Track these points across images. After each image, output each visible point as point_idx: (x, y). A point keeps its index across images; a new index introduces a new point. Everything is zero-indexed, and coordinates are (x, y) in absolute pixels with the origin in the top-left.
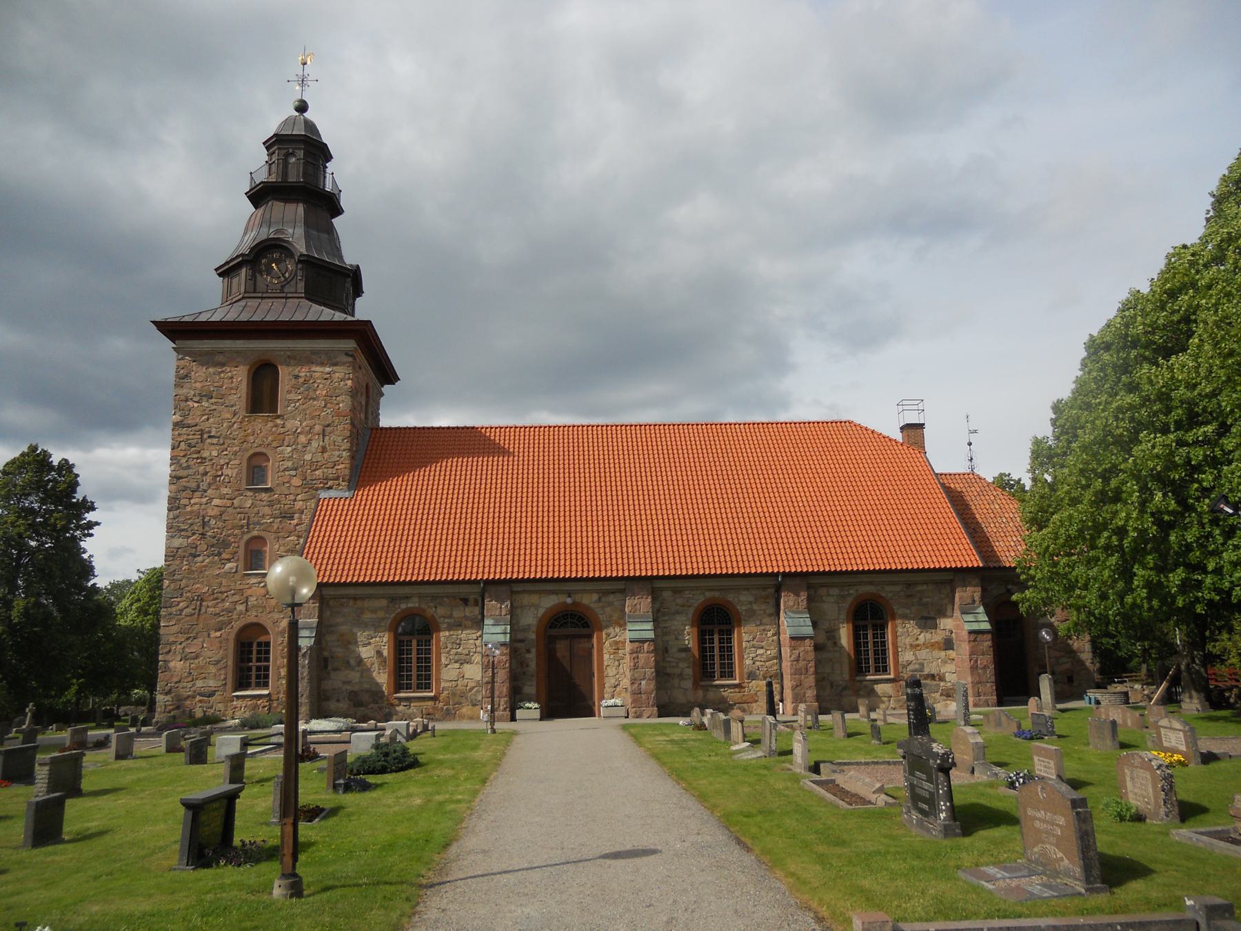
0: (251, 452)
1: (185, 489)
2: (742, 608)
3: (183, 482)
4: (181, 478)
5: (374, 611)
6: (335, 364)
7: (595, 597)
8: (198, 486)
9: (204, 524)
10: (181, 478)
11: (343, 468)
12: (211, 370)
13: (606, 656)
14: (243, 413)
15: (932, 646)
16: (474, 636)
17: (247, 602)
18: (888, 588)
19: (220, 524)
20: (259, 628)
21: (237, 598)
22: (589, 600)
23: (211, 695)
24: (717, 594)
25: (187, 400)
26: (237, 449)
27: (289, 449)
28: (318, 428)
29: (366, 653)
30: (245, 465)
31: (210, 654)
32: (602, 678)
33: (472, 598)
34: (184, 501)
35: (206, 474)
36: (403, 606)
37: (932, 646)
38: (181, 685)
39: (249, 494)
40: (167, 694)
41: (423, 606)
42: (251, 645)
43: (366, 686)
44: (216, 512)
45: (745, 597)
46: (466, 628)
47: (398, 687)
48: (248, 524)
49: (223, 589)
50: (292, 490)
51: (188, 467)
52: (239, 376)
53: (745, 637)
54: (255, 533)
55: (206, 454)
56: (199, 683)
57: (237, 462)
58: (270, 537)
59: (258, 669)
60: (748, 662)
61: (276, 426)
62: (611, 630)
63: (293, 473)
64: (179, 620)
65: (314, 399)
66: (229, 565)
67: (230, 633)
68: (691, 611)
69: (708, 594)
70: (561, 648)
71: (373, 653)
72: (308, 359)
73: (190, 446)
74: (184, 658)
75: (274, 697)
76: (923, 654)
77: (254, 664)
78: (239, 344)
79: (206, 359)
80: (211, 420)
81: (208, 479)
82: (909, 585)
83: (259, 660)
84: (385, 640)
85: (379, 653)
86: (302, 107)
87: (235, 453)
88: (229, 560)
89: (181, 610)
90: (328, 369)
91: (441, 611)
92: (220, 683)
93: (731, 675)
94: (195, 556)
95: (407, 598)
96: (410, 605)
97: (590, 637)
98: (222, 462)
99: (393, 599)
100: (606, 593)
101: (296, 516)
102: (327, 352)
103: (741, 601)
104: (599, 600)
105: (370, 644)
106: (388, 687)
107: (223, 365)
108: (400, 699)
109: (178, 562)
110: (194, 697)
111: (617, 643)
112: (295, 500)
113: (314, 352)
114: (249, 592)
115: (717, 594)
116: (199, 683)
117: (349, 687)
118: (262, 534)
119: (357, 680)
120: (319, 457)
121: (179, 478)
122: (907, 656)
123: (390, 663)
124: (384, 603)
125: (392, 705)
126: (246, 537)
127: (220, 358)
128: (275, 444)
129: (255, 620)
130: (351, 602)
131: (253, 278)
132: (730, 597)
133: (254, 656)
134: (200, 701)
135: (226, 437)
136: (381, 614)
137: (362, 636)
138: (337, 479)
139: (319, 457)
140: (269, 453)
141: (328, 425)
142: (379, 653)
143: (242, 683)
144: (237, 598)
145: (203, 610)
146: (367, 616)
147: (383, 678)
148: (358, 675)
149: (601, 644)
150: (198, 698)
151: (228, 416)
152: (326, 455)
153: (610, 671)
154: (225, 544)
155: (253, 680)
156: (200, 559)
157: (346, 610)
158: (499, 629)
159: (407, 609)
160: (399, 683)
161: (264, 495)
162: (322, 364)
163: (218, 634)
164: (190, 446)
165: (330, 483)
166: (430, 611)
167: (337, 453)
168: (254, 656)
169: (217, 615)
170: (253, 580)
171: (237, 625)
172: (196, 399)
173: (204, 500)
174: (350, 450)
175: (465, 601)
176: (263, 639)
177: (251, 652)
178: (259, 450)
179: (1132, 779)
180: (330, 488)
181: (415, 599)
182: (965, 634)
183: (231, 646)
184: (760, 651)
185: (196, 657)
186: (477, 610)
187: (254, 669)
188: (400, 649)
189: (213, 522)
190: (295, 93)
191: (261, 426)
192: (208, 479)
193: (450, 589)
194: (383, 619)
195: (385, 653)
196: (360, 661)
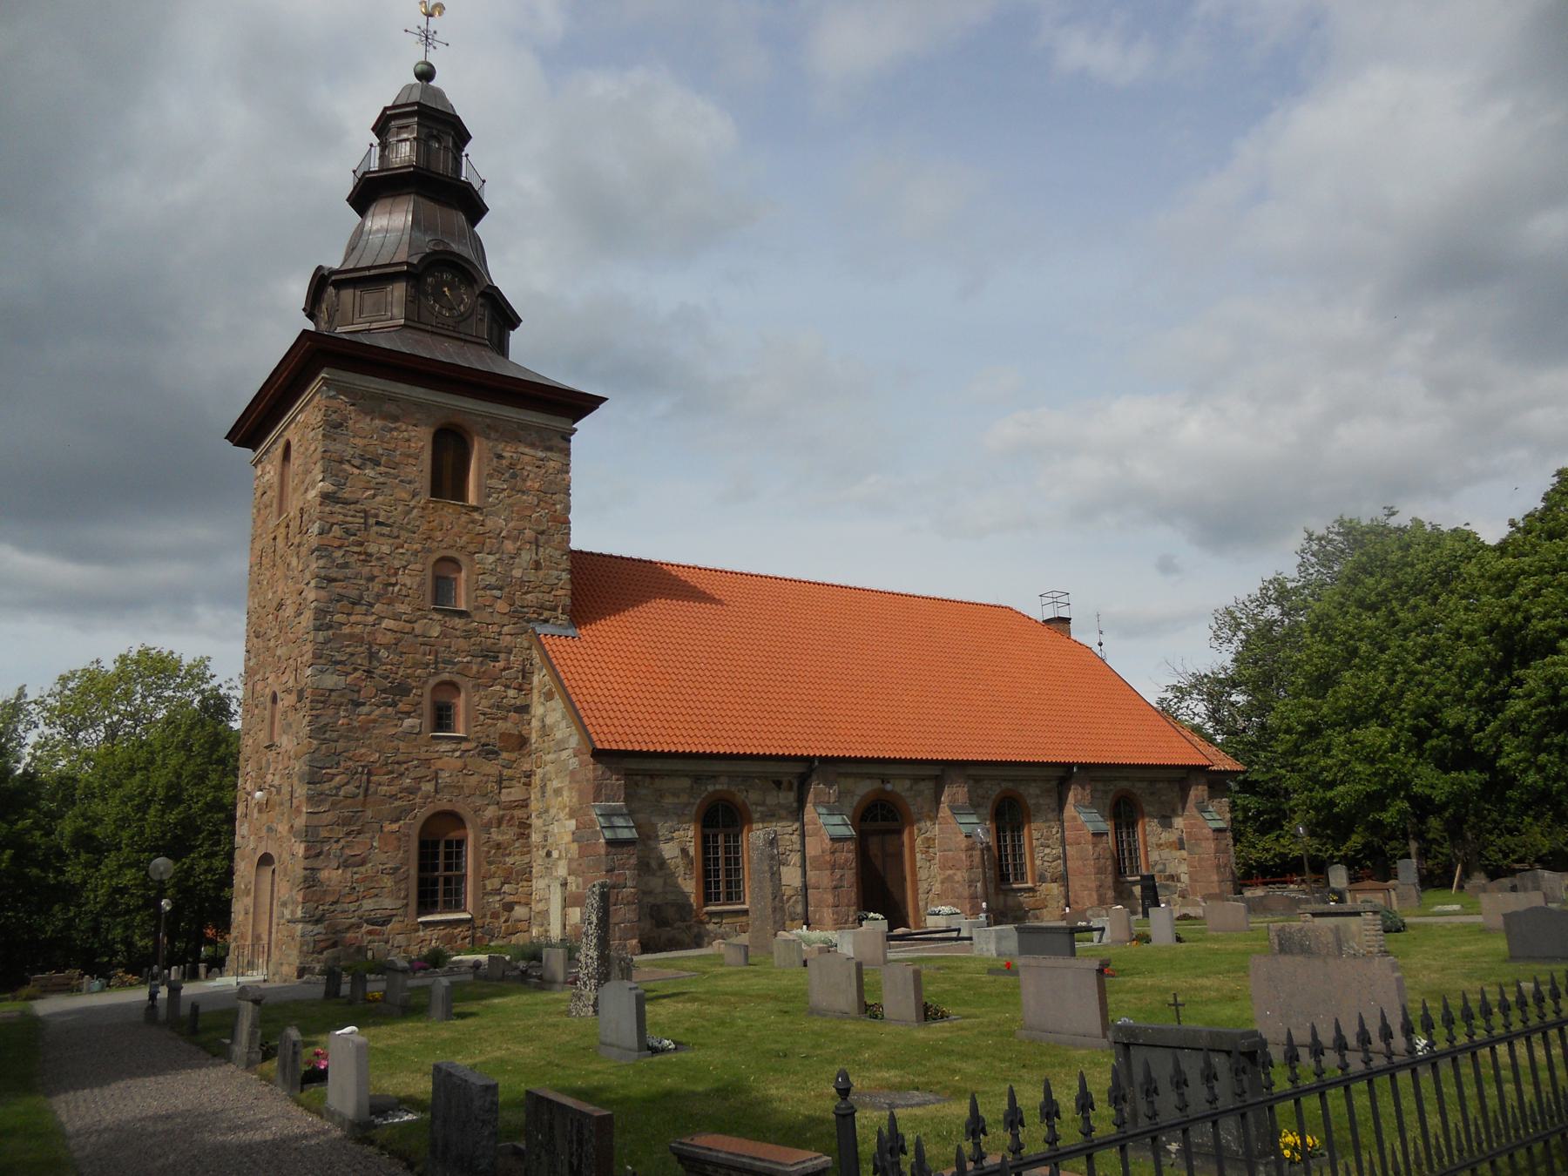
0: (437, 555)
1: (341, 597)
2: (1031, 802)
3: (337, 588)
4: (335, 580)
5: (675, 794)
6: (550, 449)
7: (907, 783)
8: (361, 597)
9: (372, 656)
10: (335, 580)
11: (563, 594)
12: (377, 422)
13: (919, 856)
14: (425, 496)
15: (1170, 845)
16: (790, 830)
17: (436, 777)
18: (1138, 785)
19: (394, 658)
20: (453, 819)
21: (421, 772)
22: (899, 787)
23: (385, 922)
24: (1010, 785)
25: (341, 462)
26: (417, 546)
27: (491, 558)
28: (529, 534)
29: (669, 851)
30: (429, 572)
31: (383, 857)
32: (915, 882)
33: (785, 780)
34: (338, 617)
35: (372, 579)
36: (710, 788)
37: (1170, 845)
38: (339, 907)
39: (437, 616)
40: (317, 922)
41: (733, 789)
42: (436, 844)
43: (671, 897)
44: (389, 638)
45: (1033, 790)
46: (781, 819)
47: (708, 897)
48: (436, 662)
49: (401, 758)
50: (497, 618)
51: (346, 565)
52: (419, 439)
53: (1036, 835)
54: (445, 676)
55: (372, 548)
56: (368, 904)
57: (418, 566)
58: (466, 684)
59: (448, 881)
60: (1038, 862)
61: (473, 522)
62: (922, 824)
63: (497, 593)
64: (334, 804)
65: (523, 492)
66: (408, 722)
67: (412, 826)
68: (990, 804)
69: (1004, 785)
70: (874, 844)
71: (677, 852)
72: (515, 434)
73: (347, 531)
74: (345, 865)
75: (479, 923)
76: (1166, 853)
77: (441, 872)
78: (419, 393)
79: (369, 404)
80: (379, 498)
81: (376, 587)
82: (1152, 781)
83: (448, 867)
84: (691, 833)
85: (684, 851)
86: (426, 74)
87: (415, 553)
88: (408, 714)
89: (338, 788)
90: (541, 454)
91: (754, 796)
92: (400, 903)
93: (1023, 880)
94: (358, 704)
95: (714, 777)
96: (718, 787)
97: (900, 832)
98: (397, 564)
99: (698, 778)
100: (917, 779)
101: (502, 656)
102: (540, 430)
103: (1032, 793)
104: (911, 789)
105: (672, 839)
106: (697, 897)
107: (395, 419)
108: (711, 914)
109: (331, 712)
110: (359, 926)
111: (928, 839)
112: (500, 634)
113: (524, 427)
114: (439, 764)
115: (1010, 785)
116: (368, 904)
117: (651, 900)
118: (456, 678)
119: (659, 890)
120: (532, 575)
121: (331, 580)
122: (1154, 856)
123: (698, 864)
124: (686, 783)
125: (702, 922)
126: (433, 682)
127: (391, 408)
128: (471, 548)
129: (448, 807)
130: (648, 781)
131: (412, 302)
132: (1022, 789)
133: (441, 861)
134: (370, 933)
135: (401, 528)
136: (684, 798)
137: (663, 829)
138: (554, 609)
139: (532, 575)
140: (463, 559)
141: (542, 533)
142: (684, 851)
143: (426, 902)
144: (421, 772)
145: (371, 790)
146: (669, 801)
147: (690, 886)
148: (661, 881)
149: (912, 840)
150: (366, 928)
151: (405, 496)
152: (541, 573)
153: (922, 874)
154: (402, 690)
155: (440, 898)
156: (365, 709)
157: (644, 791)
158: (837, 819)
159: (716, 791)
160: (708, 897)
161: (458, 622)
162: (532, 445)
163: (395, 827)
164: (347, 531)
165: (546, 614)
166: (741, 797)
167: (556, 573)
168: (441, 861)
169: (393, 797)
170: (444, 747)
171: (423, 813)
172: (357, 462)
173: (371, 619)
174: (571, 572)
175: (778, 784)
176: (454, 835)
177: (436, 856)
178: (451, 553)
179: (234, 1129)
180: (546, 621)
181: (723, 779)
182: (1207, 832)
183: (414, 846)
184: (1047, 851)
185: (363, 863)
186: (791, 797)
187: (441, 880)
188: (706, 843)
189: (383, 653)
190: (415, 54)
191: (448, 512)
192: (376, 587)
193: (772, 768)
194: (687, 805)
195: (692, 852)
196: (662, 863)
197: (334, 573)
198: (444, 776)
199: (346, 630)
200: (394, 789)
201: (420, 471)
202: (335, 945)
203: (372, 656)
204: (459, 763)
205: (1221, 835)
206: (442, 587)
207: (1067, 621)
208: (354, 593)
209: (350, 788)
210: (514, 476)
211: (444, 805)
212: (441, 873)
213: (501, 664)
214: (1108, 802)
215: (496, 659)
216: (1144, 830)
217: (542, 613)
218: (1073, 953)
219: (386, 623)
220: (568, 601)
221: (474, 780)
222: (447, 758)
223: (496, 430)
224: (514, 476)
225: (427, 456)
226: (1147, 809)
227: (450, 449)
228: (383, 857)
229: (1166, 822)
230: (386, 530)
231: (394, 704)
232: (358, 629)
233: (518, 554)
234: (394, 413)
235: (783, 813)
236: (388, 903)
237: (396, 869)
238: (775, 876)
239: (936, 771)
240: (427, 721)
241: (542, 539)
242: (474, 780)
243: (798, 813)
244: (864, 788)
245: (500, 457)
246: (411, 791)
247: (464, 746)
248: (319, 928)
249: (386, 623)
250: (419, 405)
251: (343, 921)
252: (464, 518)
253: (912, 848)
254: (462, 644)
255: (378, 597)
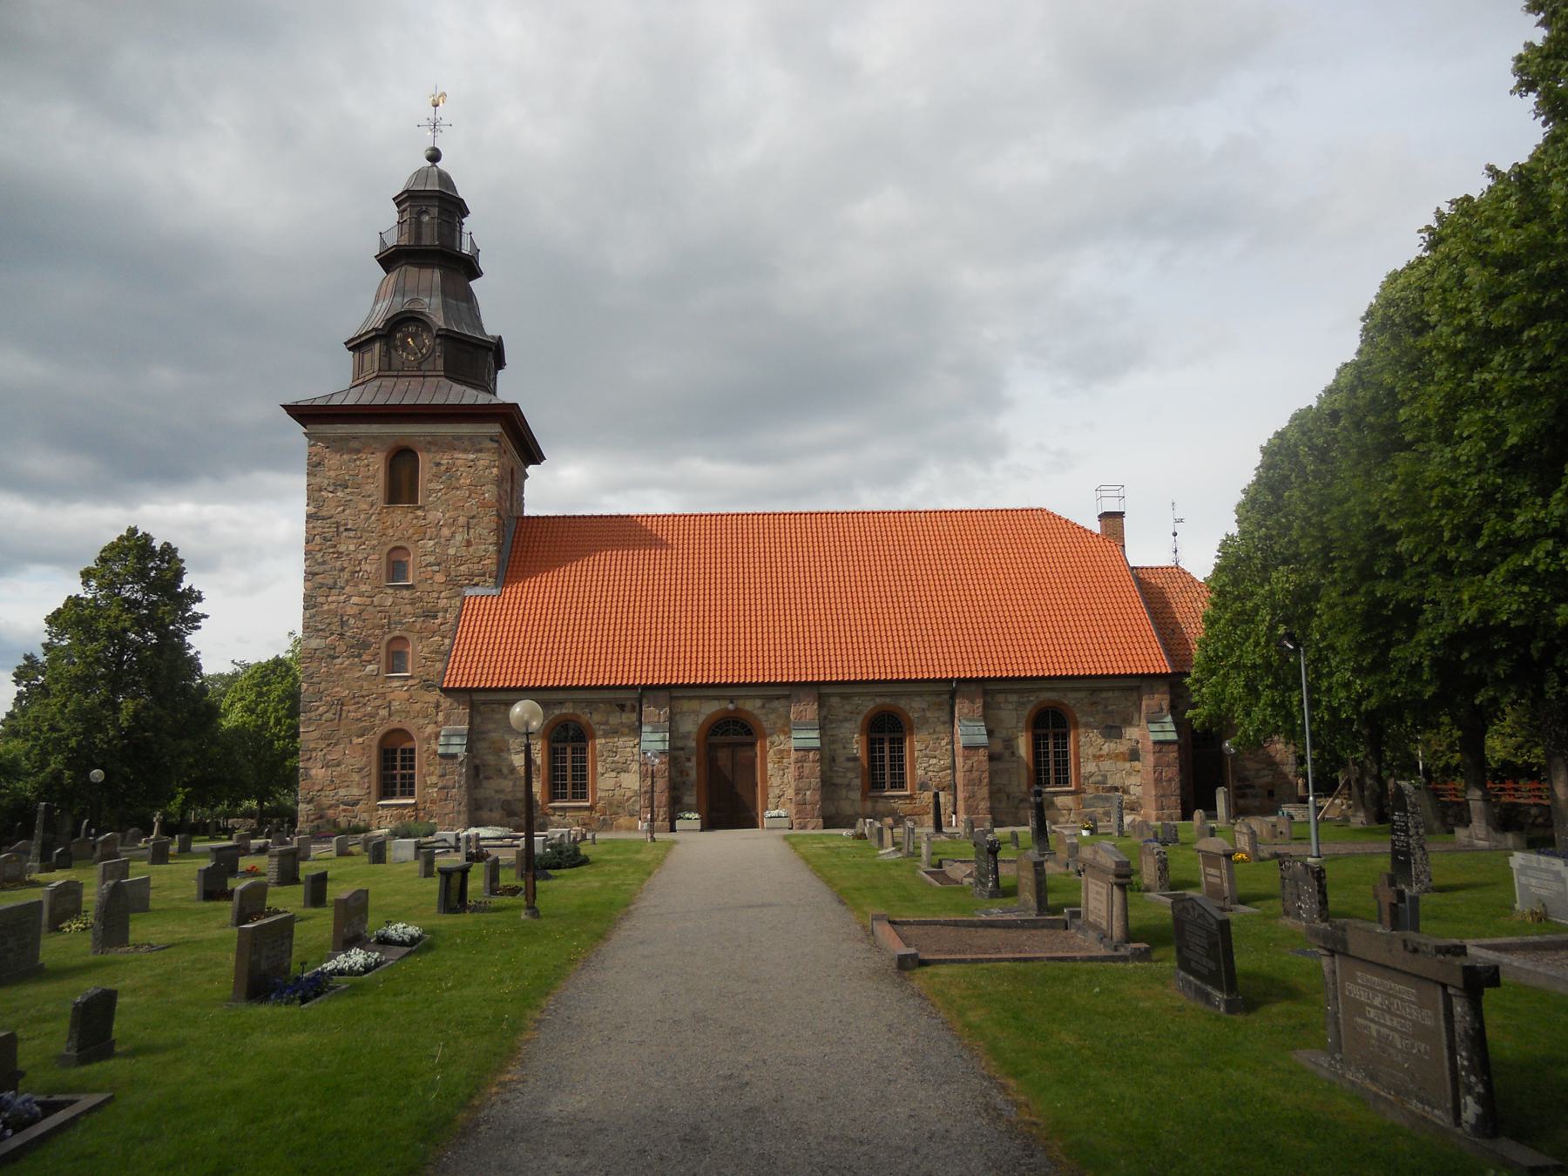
1: (321, 586)
2: (914, 715)
3: (319, 579)
6: (480, 451)
7: (759, 703)
9: (343, 624)
11: (490, 563)
12: (345, 457)
13: (770, 766)
15: (1117, 757)
19: (360, 624)
20: (403, 734)
21: (379, 702)
22: (752, 706)
28: (462, 520)
31: (352, 761)
33: (629, 703)
35: (343, 569)
36: (557, 712)
37: (1117, 757)
39: (390, 591)
41: (578, 712)
42: (395, 752)
44: (355, 610)
46: (623, 735)
47: (553, 796)
51: (324, 563)
52: (376, 464)
53: (918, 746)
54: (397, 633)
55: (342, 548)
56: (342, 792)
59: (403, 777)
60: (920, 772)
62: (775, 738)
66: (370, 667)
67: (373, 739)
68: (860, 719)
69: (878, 700)
72: (452, 445)
73: (325, 539)
74: (326, 765)
75: (421, 806)
76: (1107, 765)
81: (346, 575)
87: (374, 547)
88: (370, 662)
90: (472, 456)
91: (596, 717)
93: (902, 786)
95: (561, 703)
97: (753, 745)
98: (360, 557)
102: (471, 438)
103: (914, 708)
104: (763, 707)
107: (358, 451)
108: (555, 808)
111: (781, 751)
114: (391, 696)
116: (342, 792)
117: (503, 797)
118: (404, 634)
126: (388, 637)
127: (354, 444)
128: (415, 537)
129: (398, 726)
131: (387, 355)
132: (903, 703)
133: (398, 763)
135: (364, 530)
140: (410, 547)
143: (386, 791)
144: (379, 702)
150: (342, 807)
154: (365, 645)
155: (398, 789)
156: (339, 661)
161: (406, 593)
162: (465, 451)
164: (325, 539)
165: (476, 580)
168: (398, 763)
171: (380, 731)
173: (342, 598)
174: (496, 544)
175: (622, 708)
176: (407, 745)
177: (395, 759)
178: (398, 544)
180: (476, 585)
183: (375, 752)
184: (933, 761)
189: (352, 621)
190: (427, 141)
191: (400, 516)
192: (346, 575)
197: (316, 569)
198: (396, 705)
199: (326, 607)
200: (359, 715)
201: (376, 486)
202: (321, 817)
203: (343, 624)
204: (406, 695)
205: (1165, 748)
206: (396, 567)
207: (1121, 515)
208: (330, 582)
209: (329, 715)
210: (450, 478)
211: (396, 725)
212: (398, 772)
213: (438, 621)
214: (1026, 713)
215: (435, 617)
216: (1077, 742)
217: (472, 580)
218: (673, 829)
219: (354, 600)
220: (494, 568)
221: (417, 707)
222: (398, 692)
223: (436, 444)
224: (450, 478)
225: (381, 475)
226: (1082, 719)
227: (402, 464)
228: (352, 761)
229: (1112, 731)
230: (352, 534)
231: (360, 656)
232: (333, 606)
233: (453, 536)
234: (366, 444)
235: (626, 730)
236: (355, 791)
237: (361, 770)
238: (1482, 850)
239: (1135, 683)
240: (383, 666)
241: (473, 522)
242: (417, 707)
243: (637, 730)
244: (868, 705)
245: (438, 464)
246: (372, 716)
247: (410, 682)
248: (310, 806)
249: (354, 600)
250: (375, 438)
251: (326, 802)
252: (410, 516)
253: (764, 759)
254: (409, 609)
255: (347, 581)
